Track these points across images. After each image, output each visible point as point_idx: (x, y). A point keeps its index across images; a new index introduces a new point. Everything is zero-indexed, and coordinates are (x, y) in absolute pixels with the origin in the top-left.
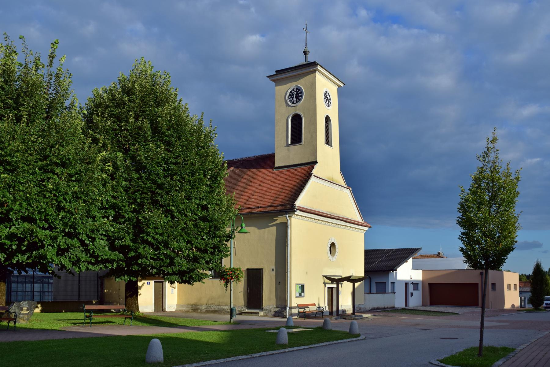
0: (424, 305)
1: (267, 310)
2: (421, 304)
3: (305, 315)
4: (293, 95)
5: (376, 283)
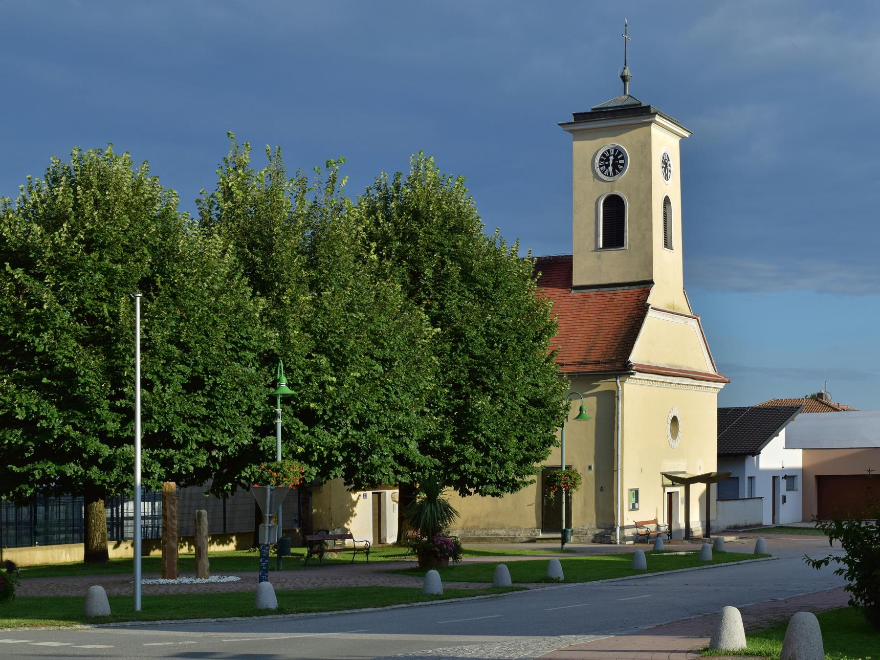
0: (804, 520)
1: (579, 533)
2: (800, 518)
3: (648, 538)
4: (608, 160)
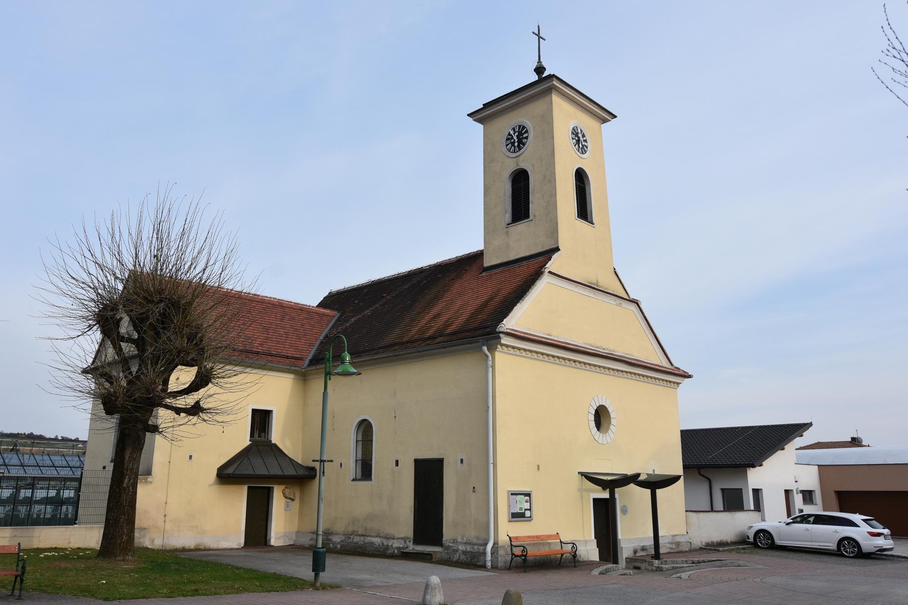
3: (525, 561)
4: (512, 138)
5: (723, 490)
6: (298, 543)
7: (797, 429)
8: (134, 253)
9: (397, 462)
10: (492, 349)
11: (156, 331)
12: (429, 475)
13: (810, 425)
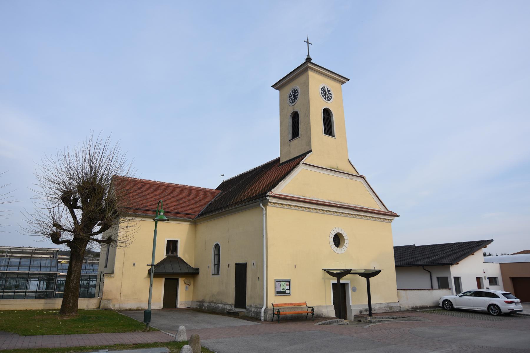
5: (438, 278)
6: (192, 307)
7: (484, 243)
8: (80, 164)
9: (295, 266)
10: (265, 205)
11: (98, 201)
12: (241, 270)
13: (492, 241)
